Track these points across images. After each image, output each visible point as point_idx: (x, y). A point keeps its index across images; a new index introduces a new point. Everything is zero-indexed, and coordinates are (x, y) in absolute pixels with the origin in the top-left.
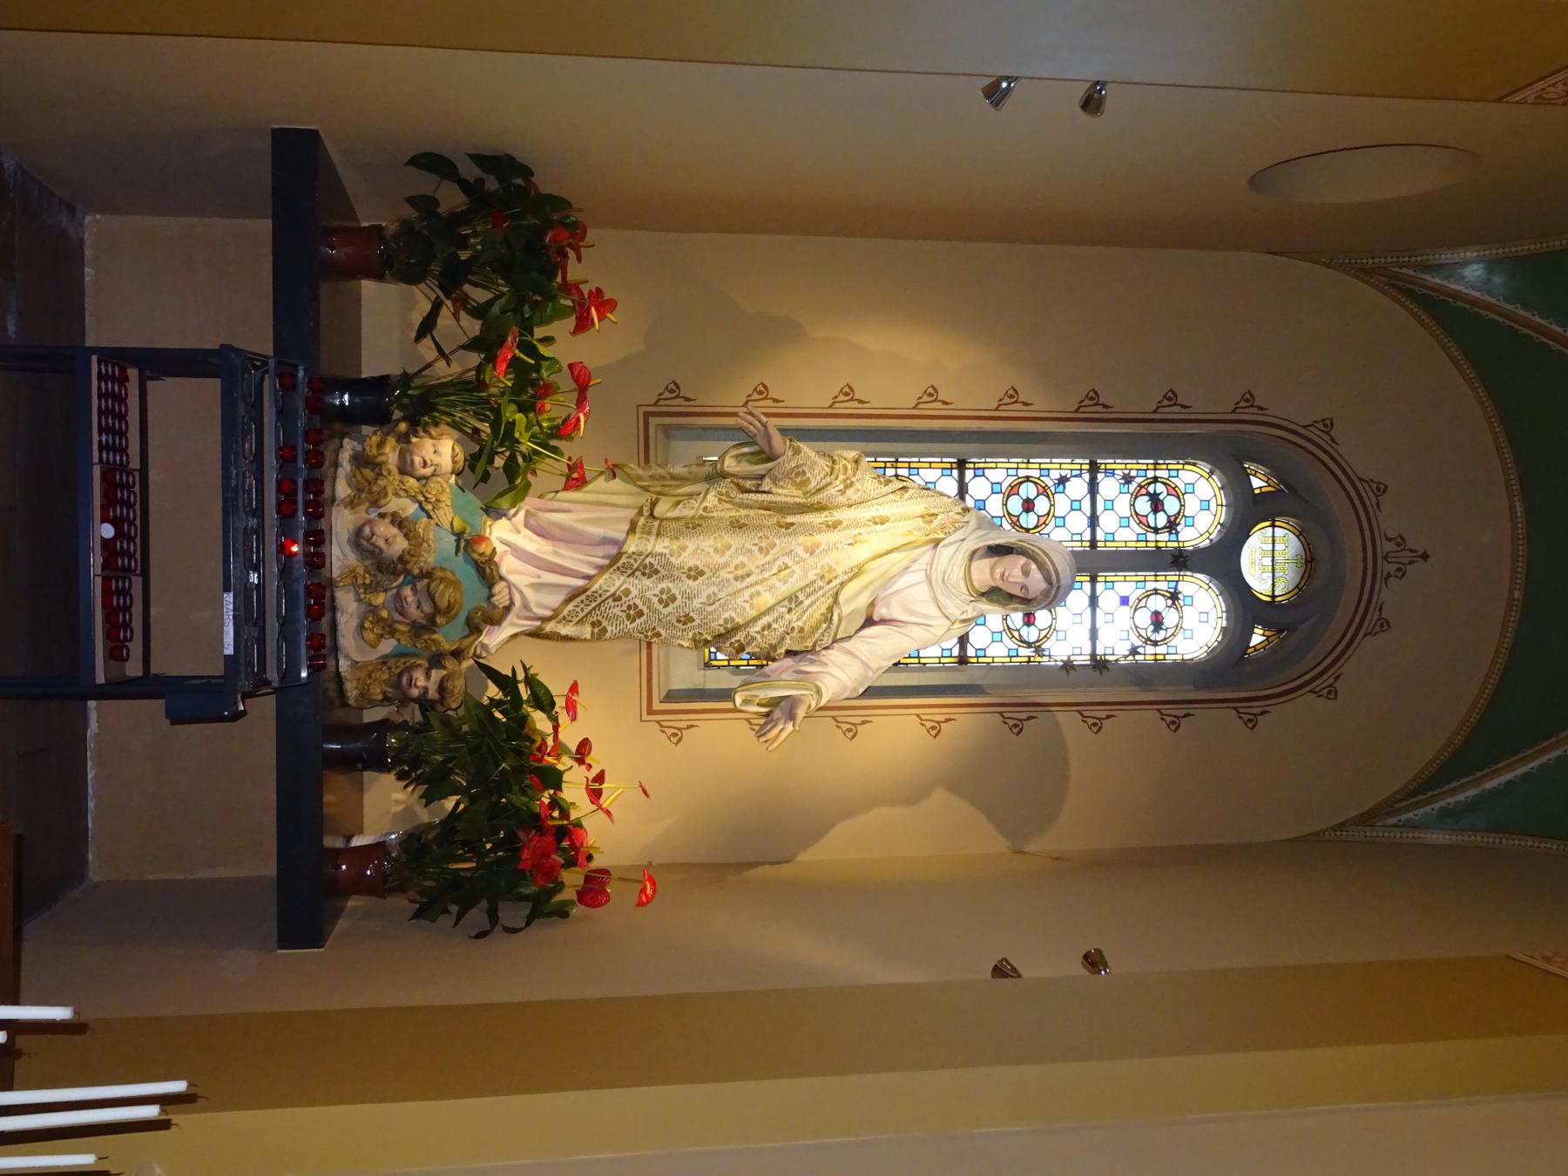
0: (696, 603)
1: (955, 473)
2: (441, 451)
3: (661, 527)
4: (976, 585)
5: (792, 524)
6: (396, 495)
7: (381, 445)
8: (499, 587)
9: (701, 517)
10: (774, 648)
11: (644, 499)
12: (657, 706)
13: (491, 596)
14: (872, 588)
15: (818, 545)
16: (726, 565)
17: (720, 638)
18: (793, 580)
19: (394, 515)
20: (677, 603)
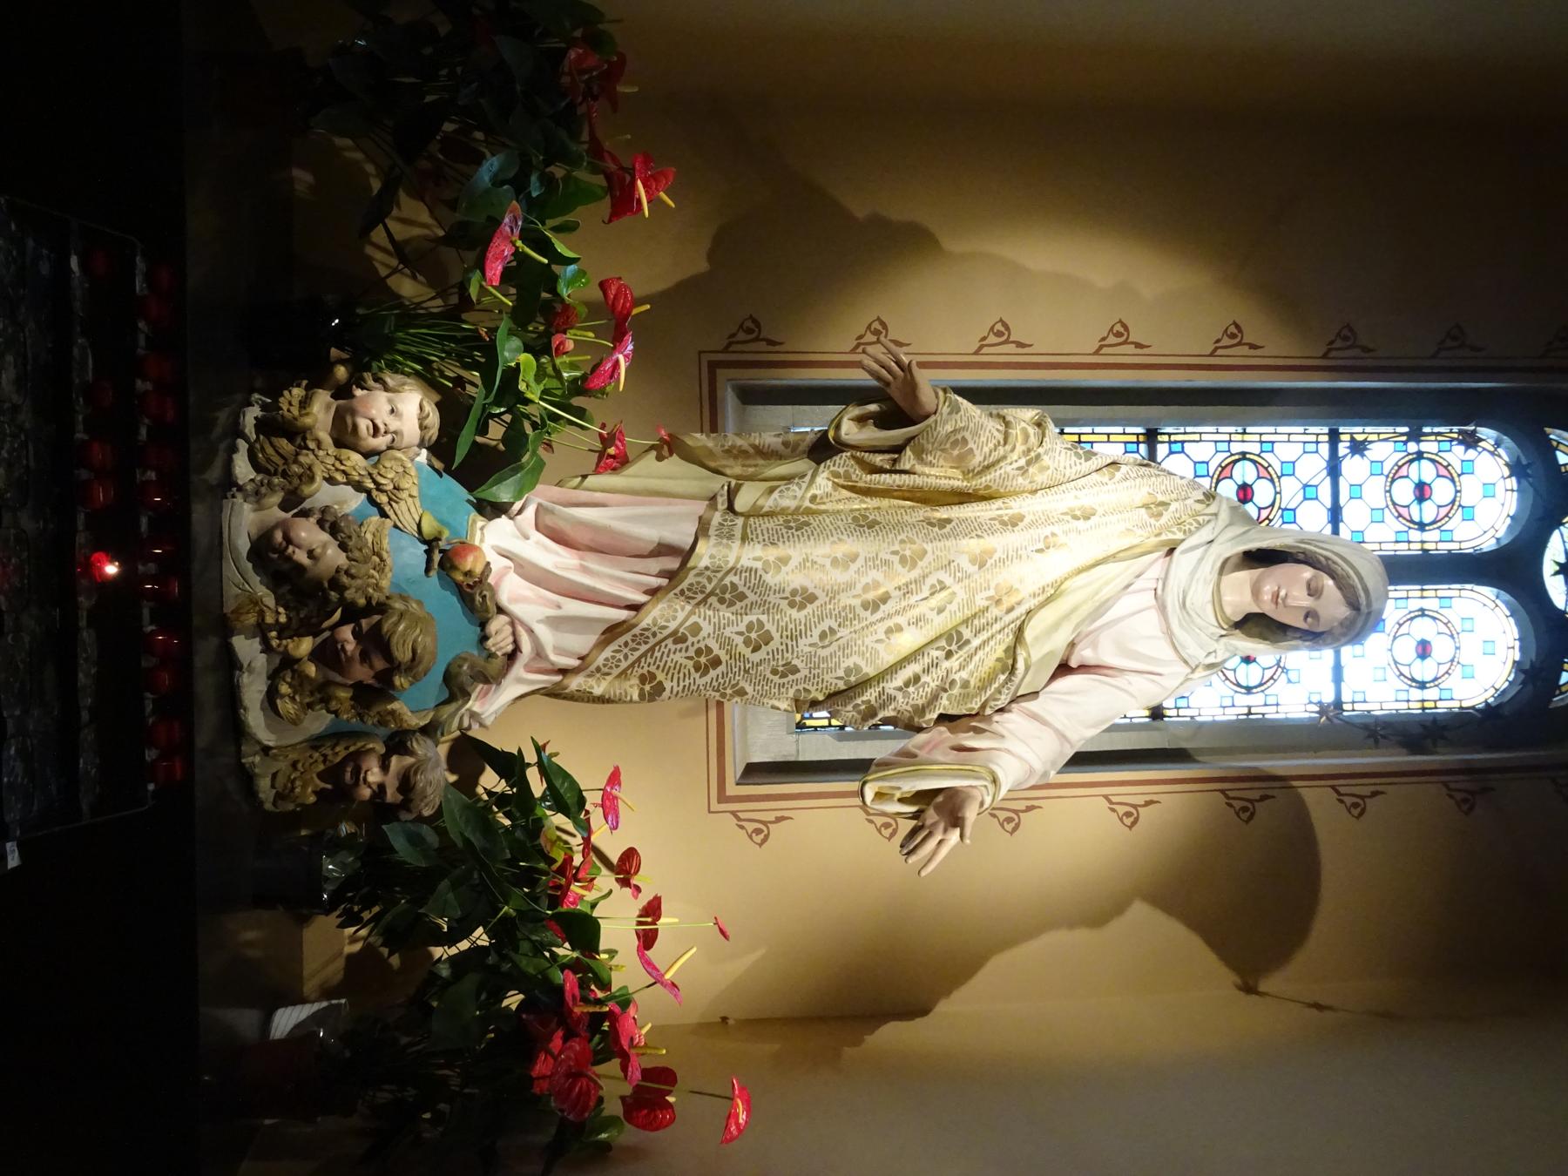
0: (804, 645)
1: (1143, 448)
2: (402, 410)
3: (749, 524)
4: (1228, 611)
5: (949, 521)
6: (331, 481)
7: (305, 403)
8: (497, 624)
9: (808, 512)
10: (921, 711)
11: (718, 484)
12: (732, 789)
13: (484, 638)
14: (1075, 619)
15: (991, 553)
16: (850, 586)
17: (835, 698)
18: (953, 607)
19: (325, 510)
20: (773, 645)
